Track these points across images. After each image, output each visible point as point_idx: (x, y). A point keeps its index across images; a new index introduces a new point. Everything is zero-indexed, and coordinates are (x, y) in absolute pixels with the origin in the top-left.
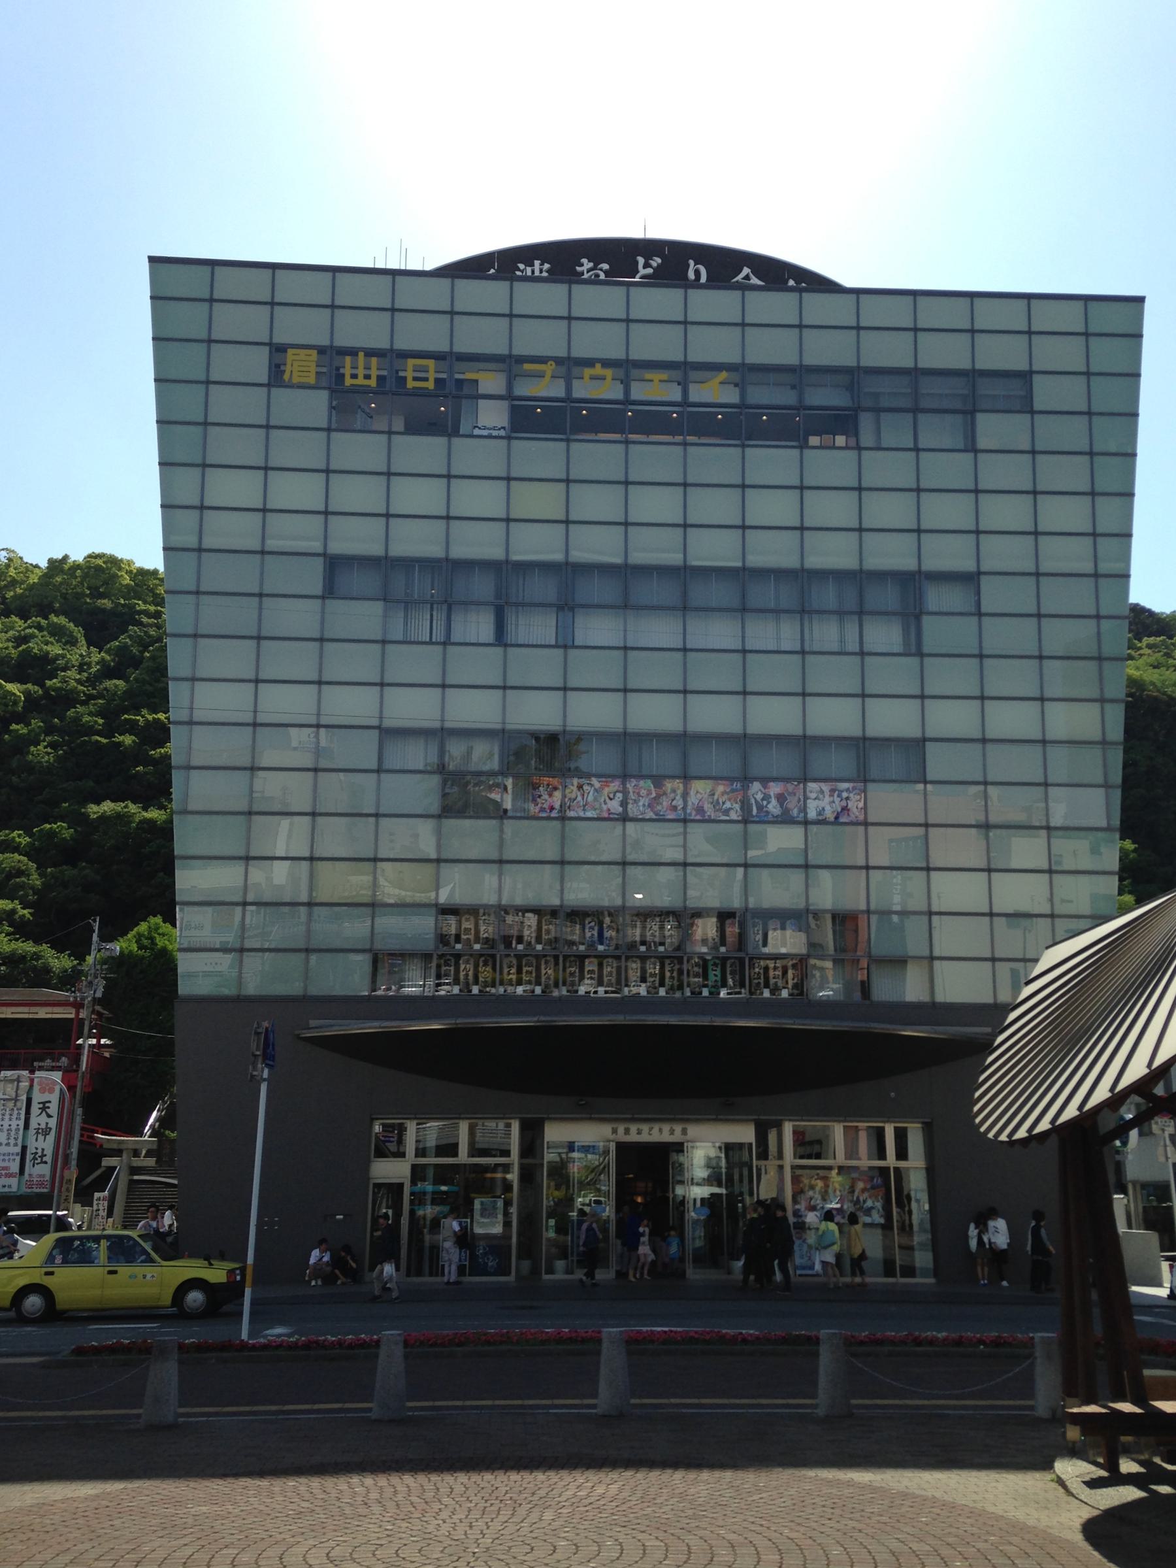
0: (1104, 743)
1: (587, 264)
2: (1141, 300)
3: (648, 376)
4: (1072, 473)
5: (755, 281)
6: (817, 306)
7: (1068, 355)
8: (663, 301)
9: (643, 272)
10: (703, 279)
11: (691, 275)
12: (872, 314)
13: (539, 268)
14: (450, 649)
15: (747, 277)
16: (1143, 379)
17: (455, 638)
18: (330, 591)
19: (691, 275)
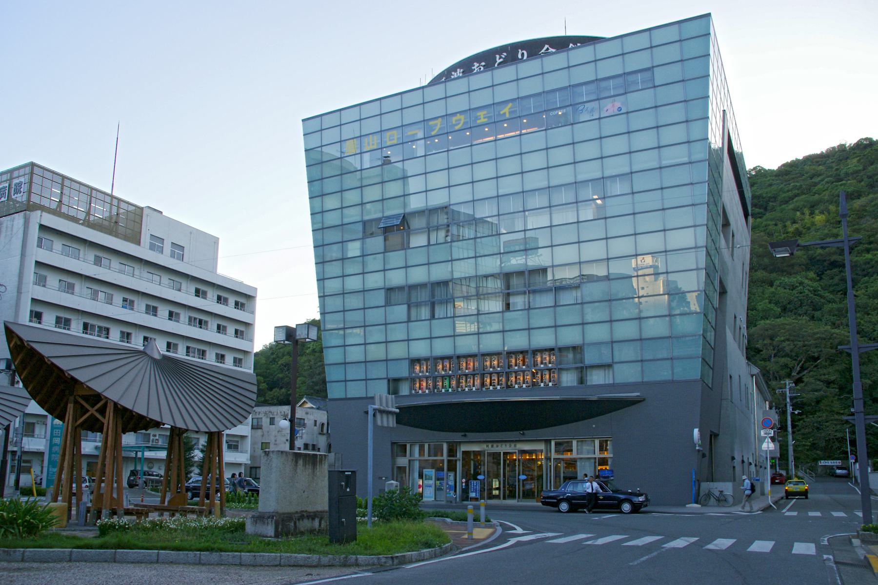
0: (697, 269)
1: (476, 65)
2: (709, 15)
3: (486, 120)
4: (677, 113)
5: (551, 50)
6: (602, 50)
7: (672, 53)
8: (507, 73)
9: (498, 61)
10: (525, 58)
11: (520, 57)
12: (630, 45)
13: (459, 72)
14: (531, 311)
15: (548, 49)
16: (305, 165)
17: (413, 318)
18: (388, 303)
19: (520, 57)
